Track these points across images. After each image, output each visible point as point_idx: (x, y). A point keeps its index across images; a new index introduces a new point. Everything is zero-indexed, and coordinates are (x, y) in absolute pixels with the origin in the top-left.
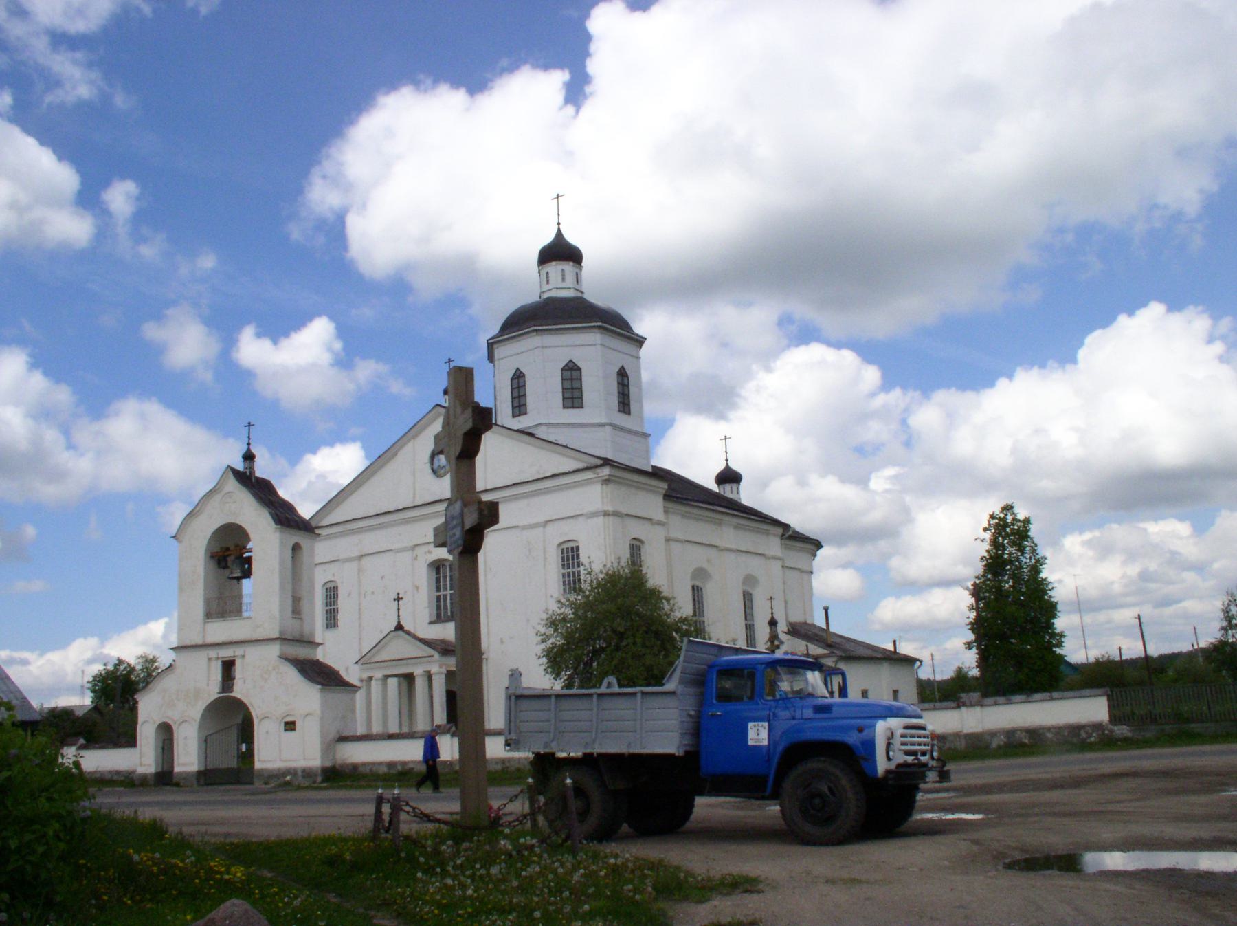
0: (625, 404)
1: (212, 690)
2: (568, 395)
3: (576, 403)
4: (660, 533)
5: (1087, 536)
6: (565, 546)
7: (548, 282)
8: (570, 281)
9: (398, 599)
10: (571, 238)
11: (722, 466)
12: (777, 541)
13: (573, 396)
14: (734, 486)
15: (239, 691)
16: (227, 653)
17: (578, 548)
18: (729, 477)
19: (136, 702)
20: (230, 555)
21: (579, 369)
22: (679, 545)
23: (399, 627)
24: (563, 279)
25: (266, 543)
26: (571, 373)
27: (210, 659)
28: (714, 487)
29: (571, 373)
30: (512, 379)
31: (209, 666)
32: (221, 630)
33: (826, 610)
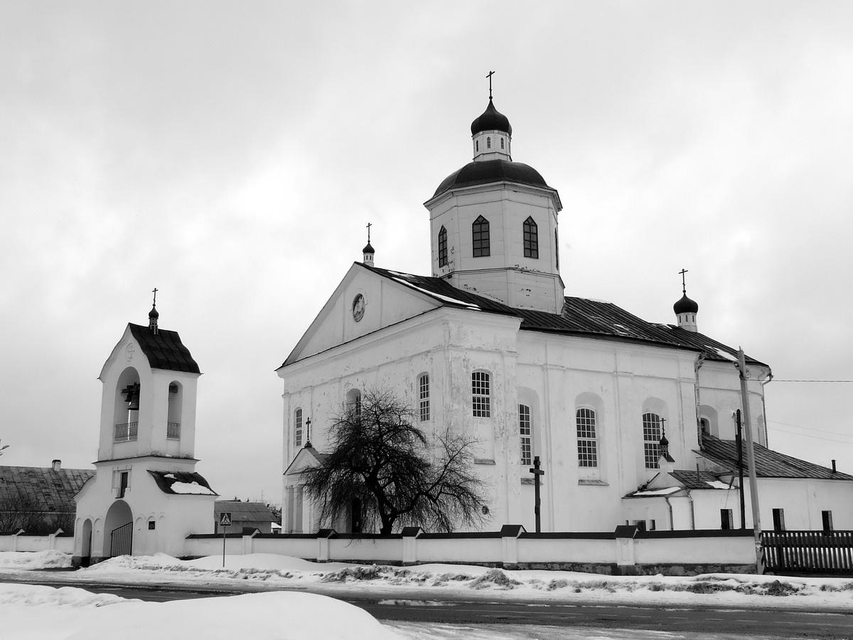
0: (531, 249)
1: (112, 498)
2: (478, 245)
3: (485, 251)
5: (406, 448)
7: (489, 146)
8: (483, 144)
10: (500, 109)
11: (679, 297)
13: (481, 245)
14: (690, 315)
15: (127, 498)
16: (122, 467)
18: (686, 306)
19: (75, 504)
20: (131, 393)
21: (488, 223)
24: (502, 147)
26: (481, 226)
27: (114, 472)
29: (481, 226)
30: (524, 223)
31: (114, 476)
32: (123, 449)
33: (193, 537)
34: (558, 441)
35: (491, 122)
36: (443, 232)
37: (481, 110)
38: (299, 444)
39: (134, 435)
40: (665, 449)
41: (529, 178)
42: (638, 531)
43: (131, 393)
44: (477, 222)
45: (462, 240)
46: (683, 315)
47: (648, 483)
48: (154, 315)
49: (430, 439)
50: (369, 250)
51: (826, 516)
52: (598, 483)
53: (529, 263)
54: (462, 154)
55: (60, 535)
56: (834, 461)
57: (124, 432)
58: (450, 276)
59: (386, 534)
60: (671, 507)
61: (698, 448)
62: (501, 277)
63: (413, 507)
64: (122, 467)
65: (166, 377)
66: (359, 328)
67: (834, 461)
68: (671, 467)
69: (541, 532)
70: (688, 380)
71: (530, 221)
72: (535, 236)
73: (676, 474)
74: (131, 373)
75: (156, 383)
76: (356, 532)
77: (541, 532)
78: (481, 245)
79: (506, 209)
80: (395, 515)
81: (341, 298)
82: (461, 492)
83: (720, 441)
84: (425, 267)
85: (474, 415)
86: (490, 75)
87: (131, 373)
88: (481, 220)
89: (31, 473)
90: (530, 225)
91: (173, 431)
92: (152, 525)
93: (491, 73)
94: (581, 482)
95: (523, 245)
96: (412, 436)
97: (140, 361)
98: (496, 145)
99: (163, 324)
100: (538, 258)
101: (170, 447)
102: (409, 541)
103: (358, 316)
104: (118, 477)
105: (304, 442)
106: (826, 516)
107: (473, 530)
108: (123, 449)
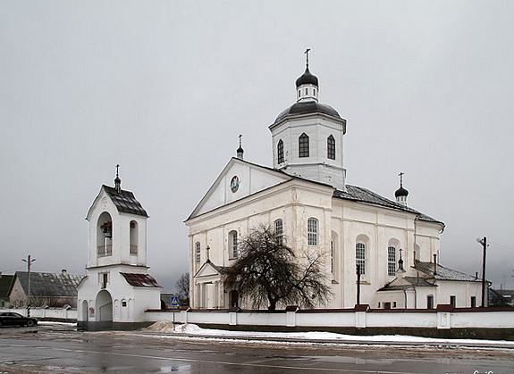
0: (332, 154)
4: (328, 214)
8: (311, 94)
9: (208, 249)
10: (312, 73)
12: (330, 198)
13: (304, 152)
16: (104, 271)
18: (402, 193)
20: (106, 226)
22: (383, 228)
23: (209, 261)
25: (121, 222)
26: (304, 139)
28: (393, 199)
29: (304, 139)
33: (149, 311)
35: (307, 80)
36: (281, 143)
38: (198, 261)
39: (110, 252)
41: (330, 114)
42: (387, 308)
43: (106, 226)
45: (292, 147)
46: (400, 197)
48: (118, 181)
49: (297, 254)
50: (240, 151)
51: (453, 298)
53: (330, 162)
54: (291, 97)
55: (69, 309)
57: (103, 250)
58: (285, 168)
59: (272, 310)
62: (315, 169)
63: (286, 295)
64: (104, 271)
65: (128, 218)
66: (235, 197)
68: (404, 275)
69: (512, 313)
70: (411, 230)
73: (406, 278)
74: (106, 215)
75: (121, 222)
76: (234, 307)
77: (512, 313)
78: (304, 152)
80: (277, 299)
81: (224, 179)
82: (320, 289)
84: (271, 162)
87: (106, 215)
89: (50, 276)
90: (331, 139)
91: (133, 251)
92: (124, 304)
96: (286, 251)
97: (109, 206)
98: (311, 94)
99: (123, 187)
101: (133, 260)
102: (291, 315)
103: (234, 189)
104: (102, 276)
105: (203, 260)
106: (453, 298)
107: (322, 307)
108: (103, 261)
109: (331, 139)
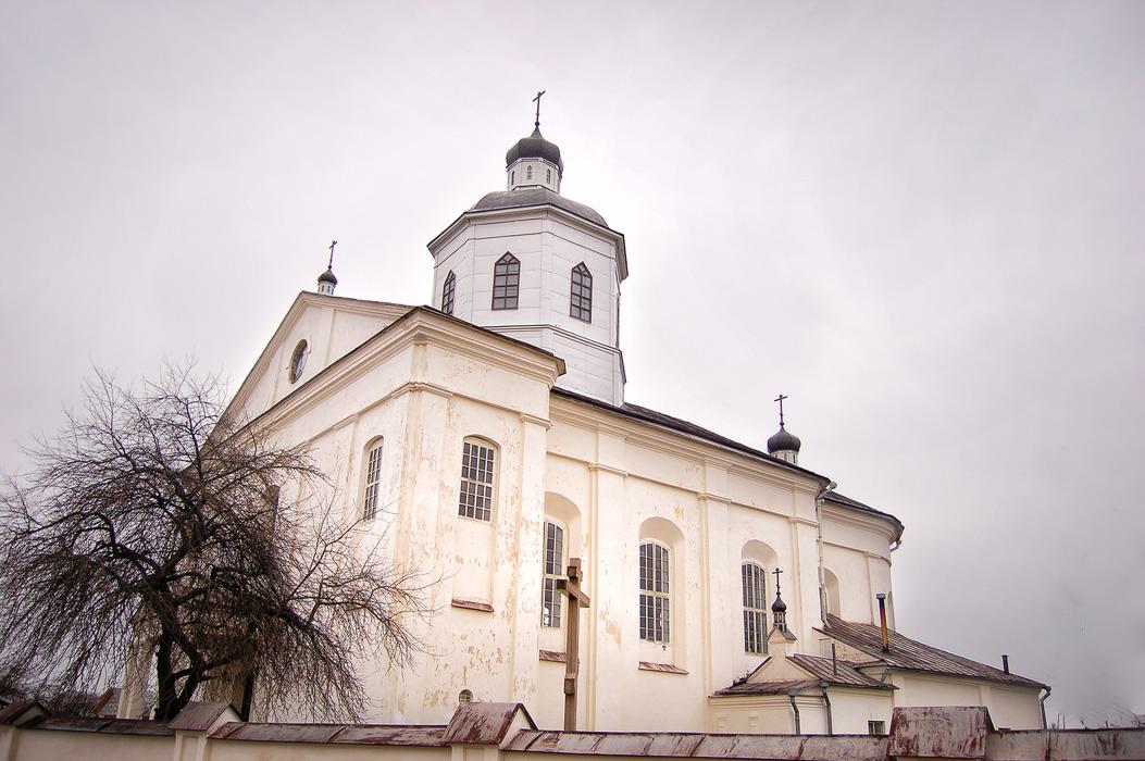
0: (582, 306)
3: (510, 302)
6: (472, 442)
17: (491, 452)
21: (518, 262)
24: (548, 181)
26: (508, 266)
29: (508, 266)
30: (573, 270)
34: (614, 591)
35: (535, 150)
37: (527, 133)
40: (781, 618)
44: (502, 262)
47: (749, 676)
52: (669, 669)
53: (576, 327)
56: (1005, 657)
60: (797, 712)
61: (820, 626)
67: (1005, 657)
71: (583, 269)
72: (587, 313)
73: (796, 660)
79: (548, 255)
83: (844, 622)
85: (461, 512)
86: (538, 98)
88: (508, 258)
90: (581, 271)
93: (540, 94)
94: (645, 666)
95: (569, 300)
100: (590, 322)
109: (581, 271)
